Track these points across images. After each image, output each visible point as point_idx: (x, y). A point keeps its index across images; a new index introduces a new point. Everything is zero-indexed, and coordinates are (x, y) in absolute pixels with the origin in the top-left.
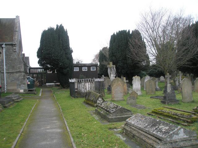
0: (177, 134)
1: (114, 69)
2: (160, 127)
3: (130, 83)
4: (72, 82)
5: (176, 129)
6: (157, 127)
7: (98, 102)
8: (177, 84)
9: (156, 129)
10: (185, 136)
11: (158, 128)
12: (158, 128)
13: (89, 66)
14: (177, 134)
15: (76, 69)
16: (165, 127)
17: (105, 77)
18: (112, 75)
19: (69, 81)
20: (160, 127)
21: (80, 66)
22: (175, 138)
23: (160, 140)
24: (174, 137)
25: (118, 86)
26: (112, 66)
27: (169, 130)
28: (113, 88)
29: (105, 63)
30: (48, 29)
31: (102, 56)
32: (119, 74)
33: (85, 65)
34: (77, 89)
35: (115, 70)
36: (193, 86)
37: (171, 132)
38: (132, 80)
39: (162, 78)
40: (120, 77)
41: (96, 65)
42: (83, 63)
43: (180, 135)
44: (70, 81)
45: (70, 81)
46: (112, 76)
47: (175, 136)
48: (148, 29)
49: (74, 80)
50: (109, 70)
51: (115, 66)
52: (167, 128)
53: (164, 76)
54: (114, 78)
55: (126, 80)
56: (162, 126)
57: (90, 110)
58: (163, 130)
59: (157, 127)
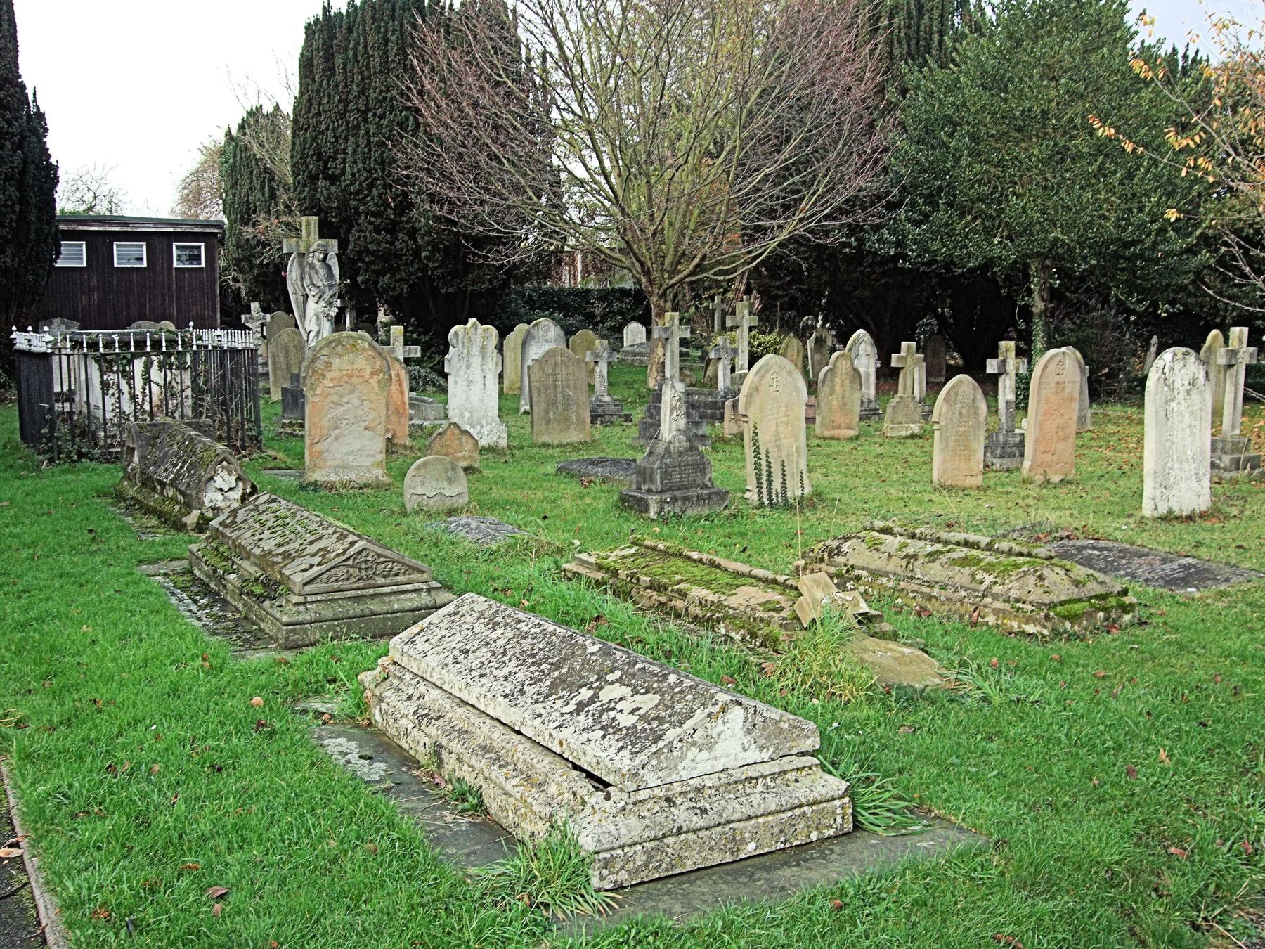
0: (709, 745)
1: (329, 268)
2: (606, 694)
3: (430, 372)
4: (34, 349)
5: (700, 714)
6: (585, 694)
7: (211, 497)
8: (721, 385)
9: (581, 707)
10: (753, 755)
11: (592, 700)
12: (592, 700)
13: (159, 239)
14: (709, 745)
15: (73, 256)
16: (637, 697)
17: (268, 316)
18: (313, 307)
19: (11, 343)
20: (606, 694)
21: (102, 234)
22: (696, 766)
23: (601, 784)
24: (686, 762)
25: (349, 391)
26: (316, 242)
27: (660, 720)
28: (313, 399)
29: (266, 225)
30: (481, 242)
31: (238, 162)
32: (357, 306)
33: (129, 231)
34: (69, 397)
35: (337, 272)
36: (813, 400)
37: (672, 734)
38: (445, 347)
39: (634, 333)
40: (366, 320)
41: (211, 237)
42: (128, 211)
43: (719, 748)
44: (21, 340)
45: (21, 340)
46: (314, 314)
47: (690, 755)
48: (562, 14)
49: (49, 338)
50: (292, 274)
51: (334, 244)
52: (648, 702)
53: (646, 321)
54: (327, 326)
55: (406, 342)
56: (617, 691)
57: (478, 84)
58: (626, 720)
59: (585, 694)
